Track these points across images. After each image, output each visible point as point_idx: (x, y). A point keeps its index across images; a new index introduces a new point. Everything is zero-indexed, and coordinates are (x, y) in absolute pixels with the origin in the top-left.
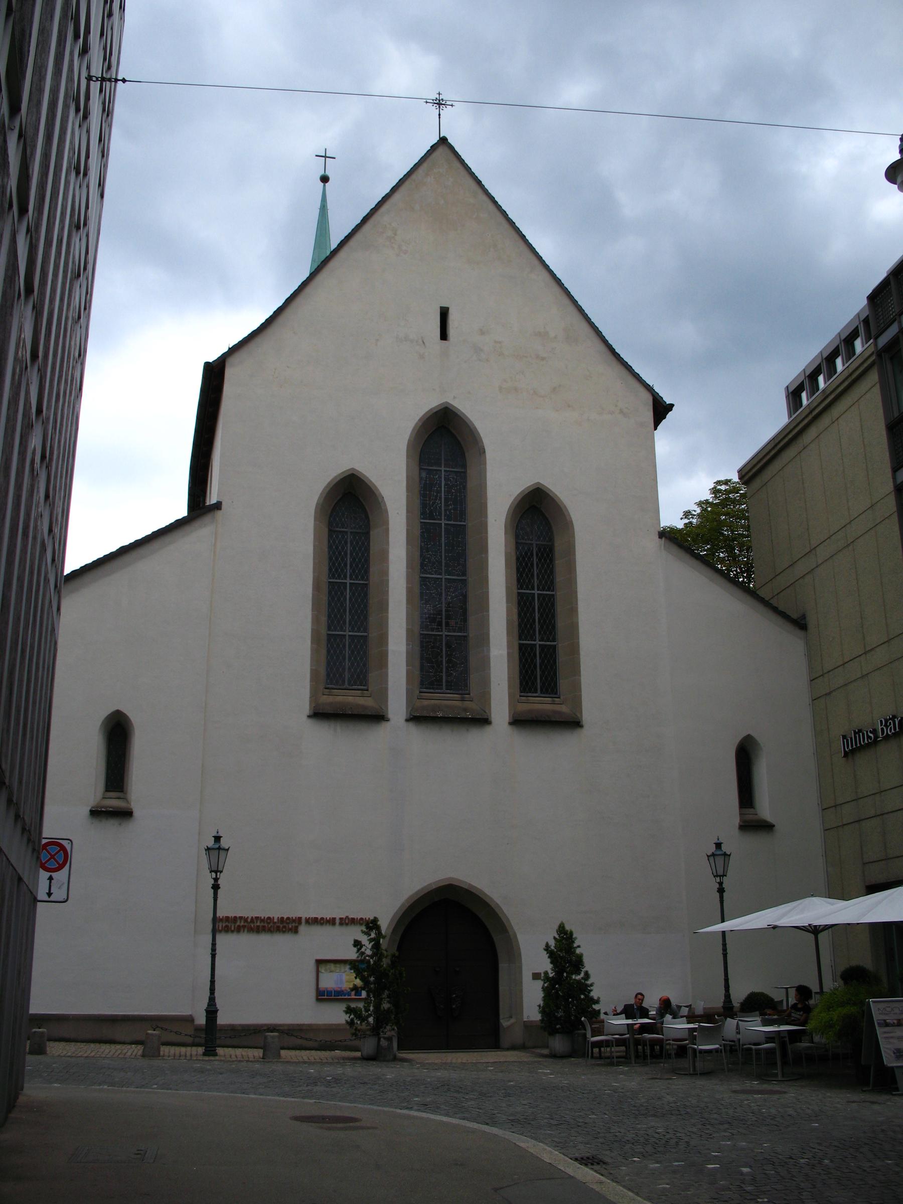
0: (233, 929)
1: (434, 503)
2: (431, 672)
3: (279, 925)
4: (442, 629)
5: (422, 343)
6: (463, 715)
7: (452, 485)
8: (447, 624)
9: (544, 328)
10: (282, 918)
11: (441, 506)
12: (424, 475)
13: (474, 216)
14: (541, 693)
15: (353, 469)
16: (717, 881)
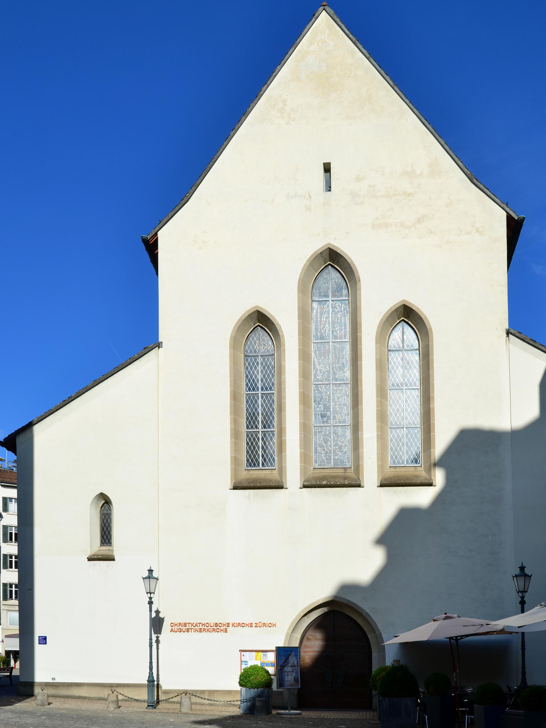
0: (184, 631)
2: (323, 454)
3: (215, 627)
6: (342, 482)
7: (338, 311)
13: (352, 75)
16: (520, 596)
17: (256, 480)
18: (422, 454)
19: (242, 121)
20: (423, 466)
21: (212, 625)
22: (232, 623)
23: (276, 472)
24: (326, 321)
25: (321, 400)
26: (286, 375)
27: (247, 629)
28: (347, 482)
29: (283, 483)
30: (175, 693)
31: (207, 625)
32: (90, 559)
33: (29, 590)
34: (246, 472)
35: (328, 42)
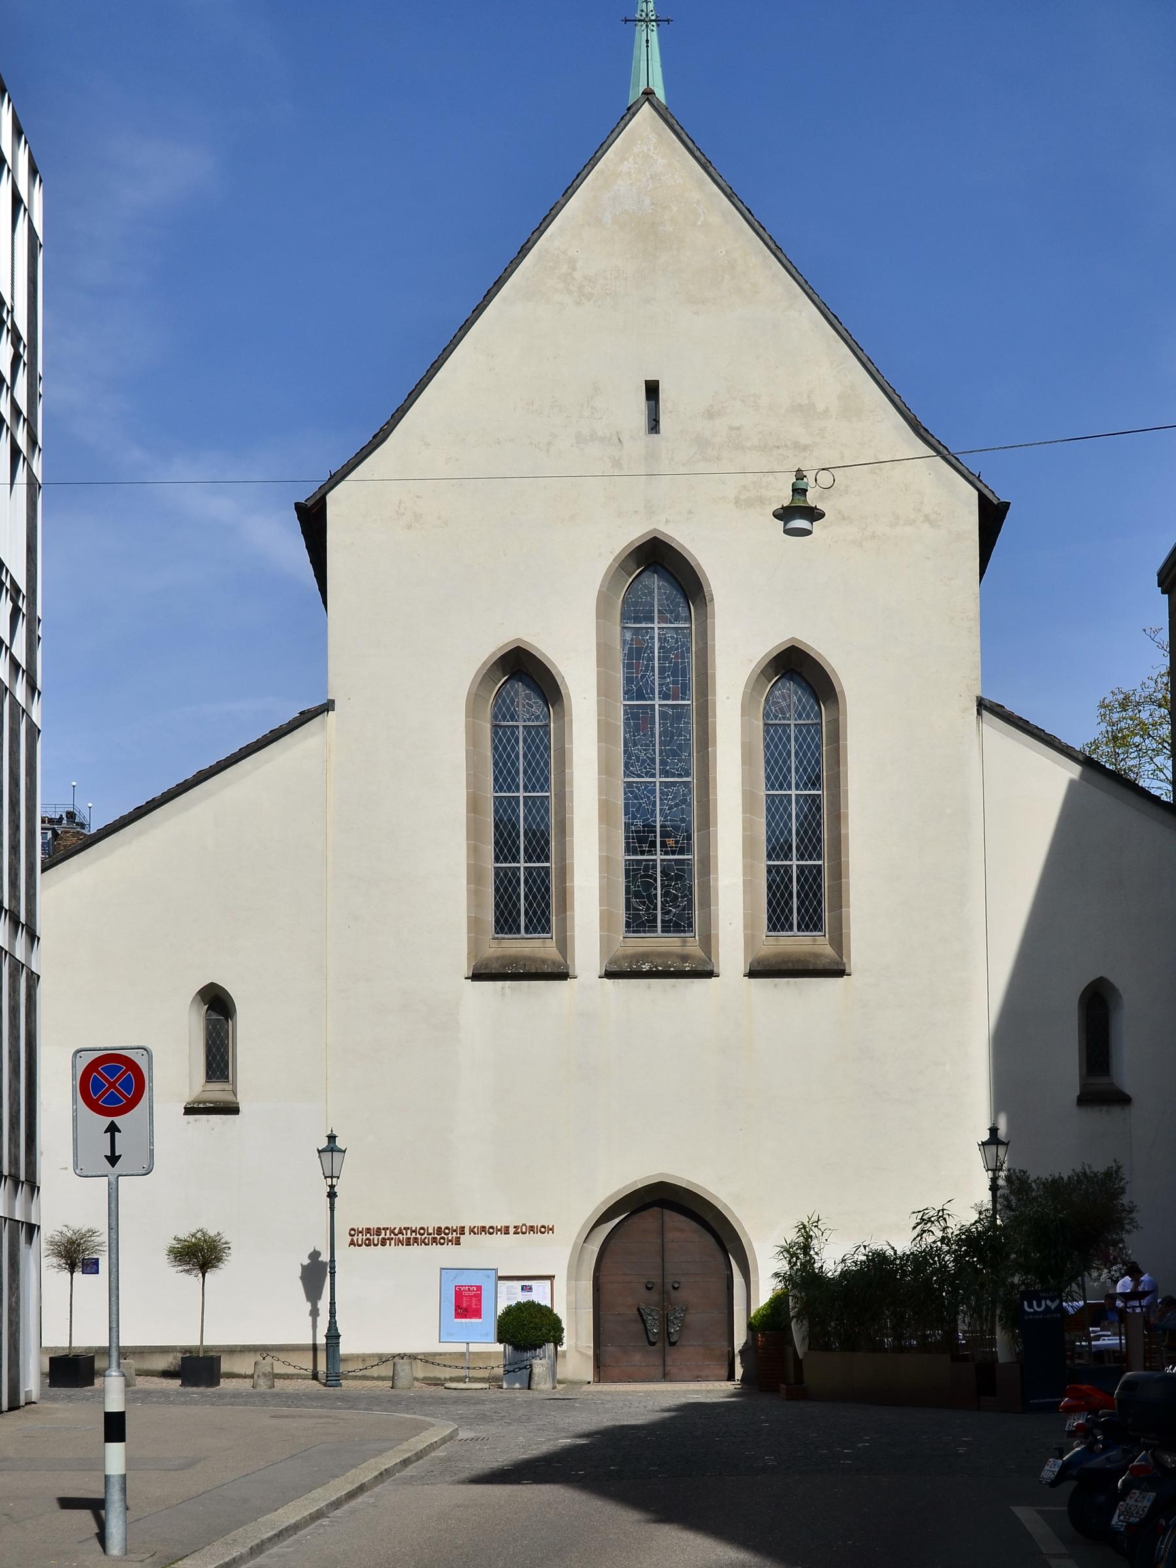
1: (643, 676)
3: (436, 1236)
4: (656, 851)
5: (617, 440)
8: (663, 844)
9: (809, 397)
10: (440, 1228)
11: (654, 679)
12: (628, 636)
13: (699, 223)
14: (799, 930)
15: (519, 639)
17: (515, 960)
18: (827, 914)
19: (490, 296)
20: (827, 936)
21: (431, 1231)
22: (470, 1227)
23: (553, 943)
24: (648, 665)
25: (638, 810)
26: (574, 768)
27: (499, 1237)
28: (688, 966)
29: (567, 967)
30: (357, 1360)
31: (422, 1231)
32: (189, 1111)
33: (62, 1169)
34: (494, 943)
35: (655, 157)
